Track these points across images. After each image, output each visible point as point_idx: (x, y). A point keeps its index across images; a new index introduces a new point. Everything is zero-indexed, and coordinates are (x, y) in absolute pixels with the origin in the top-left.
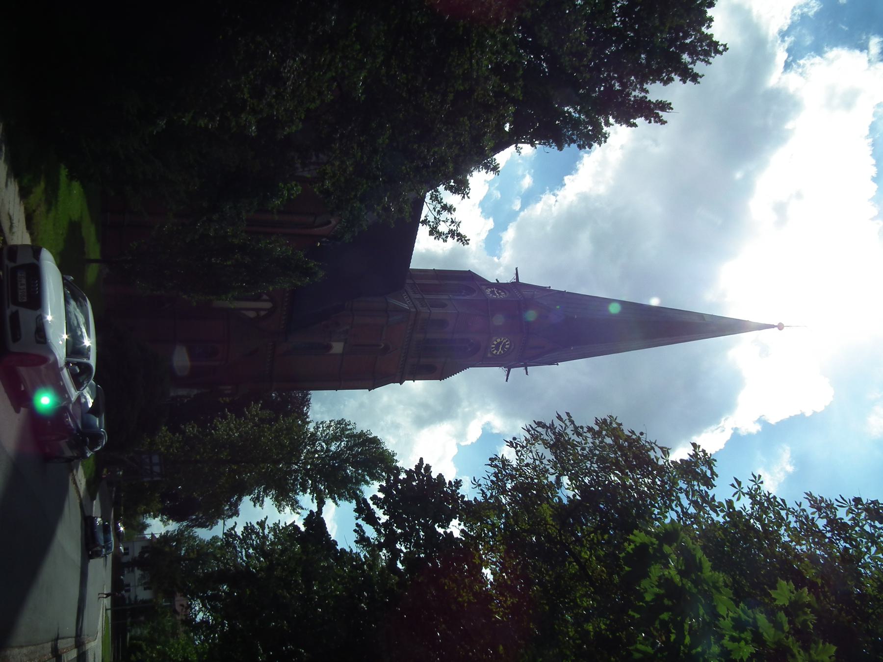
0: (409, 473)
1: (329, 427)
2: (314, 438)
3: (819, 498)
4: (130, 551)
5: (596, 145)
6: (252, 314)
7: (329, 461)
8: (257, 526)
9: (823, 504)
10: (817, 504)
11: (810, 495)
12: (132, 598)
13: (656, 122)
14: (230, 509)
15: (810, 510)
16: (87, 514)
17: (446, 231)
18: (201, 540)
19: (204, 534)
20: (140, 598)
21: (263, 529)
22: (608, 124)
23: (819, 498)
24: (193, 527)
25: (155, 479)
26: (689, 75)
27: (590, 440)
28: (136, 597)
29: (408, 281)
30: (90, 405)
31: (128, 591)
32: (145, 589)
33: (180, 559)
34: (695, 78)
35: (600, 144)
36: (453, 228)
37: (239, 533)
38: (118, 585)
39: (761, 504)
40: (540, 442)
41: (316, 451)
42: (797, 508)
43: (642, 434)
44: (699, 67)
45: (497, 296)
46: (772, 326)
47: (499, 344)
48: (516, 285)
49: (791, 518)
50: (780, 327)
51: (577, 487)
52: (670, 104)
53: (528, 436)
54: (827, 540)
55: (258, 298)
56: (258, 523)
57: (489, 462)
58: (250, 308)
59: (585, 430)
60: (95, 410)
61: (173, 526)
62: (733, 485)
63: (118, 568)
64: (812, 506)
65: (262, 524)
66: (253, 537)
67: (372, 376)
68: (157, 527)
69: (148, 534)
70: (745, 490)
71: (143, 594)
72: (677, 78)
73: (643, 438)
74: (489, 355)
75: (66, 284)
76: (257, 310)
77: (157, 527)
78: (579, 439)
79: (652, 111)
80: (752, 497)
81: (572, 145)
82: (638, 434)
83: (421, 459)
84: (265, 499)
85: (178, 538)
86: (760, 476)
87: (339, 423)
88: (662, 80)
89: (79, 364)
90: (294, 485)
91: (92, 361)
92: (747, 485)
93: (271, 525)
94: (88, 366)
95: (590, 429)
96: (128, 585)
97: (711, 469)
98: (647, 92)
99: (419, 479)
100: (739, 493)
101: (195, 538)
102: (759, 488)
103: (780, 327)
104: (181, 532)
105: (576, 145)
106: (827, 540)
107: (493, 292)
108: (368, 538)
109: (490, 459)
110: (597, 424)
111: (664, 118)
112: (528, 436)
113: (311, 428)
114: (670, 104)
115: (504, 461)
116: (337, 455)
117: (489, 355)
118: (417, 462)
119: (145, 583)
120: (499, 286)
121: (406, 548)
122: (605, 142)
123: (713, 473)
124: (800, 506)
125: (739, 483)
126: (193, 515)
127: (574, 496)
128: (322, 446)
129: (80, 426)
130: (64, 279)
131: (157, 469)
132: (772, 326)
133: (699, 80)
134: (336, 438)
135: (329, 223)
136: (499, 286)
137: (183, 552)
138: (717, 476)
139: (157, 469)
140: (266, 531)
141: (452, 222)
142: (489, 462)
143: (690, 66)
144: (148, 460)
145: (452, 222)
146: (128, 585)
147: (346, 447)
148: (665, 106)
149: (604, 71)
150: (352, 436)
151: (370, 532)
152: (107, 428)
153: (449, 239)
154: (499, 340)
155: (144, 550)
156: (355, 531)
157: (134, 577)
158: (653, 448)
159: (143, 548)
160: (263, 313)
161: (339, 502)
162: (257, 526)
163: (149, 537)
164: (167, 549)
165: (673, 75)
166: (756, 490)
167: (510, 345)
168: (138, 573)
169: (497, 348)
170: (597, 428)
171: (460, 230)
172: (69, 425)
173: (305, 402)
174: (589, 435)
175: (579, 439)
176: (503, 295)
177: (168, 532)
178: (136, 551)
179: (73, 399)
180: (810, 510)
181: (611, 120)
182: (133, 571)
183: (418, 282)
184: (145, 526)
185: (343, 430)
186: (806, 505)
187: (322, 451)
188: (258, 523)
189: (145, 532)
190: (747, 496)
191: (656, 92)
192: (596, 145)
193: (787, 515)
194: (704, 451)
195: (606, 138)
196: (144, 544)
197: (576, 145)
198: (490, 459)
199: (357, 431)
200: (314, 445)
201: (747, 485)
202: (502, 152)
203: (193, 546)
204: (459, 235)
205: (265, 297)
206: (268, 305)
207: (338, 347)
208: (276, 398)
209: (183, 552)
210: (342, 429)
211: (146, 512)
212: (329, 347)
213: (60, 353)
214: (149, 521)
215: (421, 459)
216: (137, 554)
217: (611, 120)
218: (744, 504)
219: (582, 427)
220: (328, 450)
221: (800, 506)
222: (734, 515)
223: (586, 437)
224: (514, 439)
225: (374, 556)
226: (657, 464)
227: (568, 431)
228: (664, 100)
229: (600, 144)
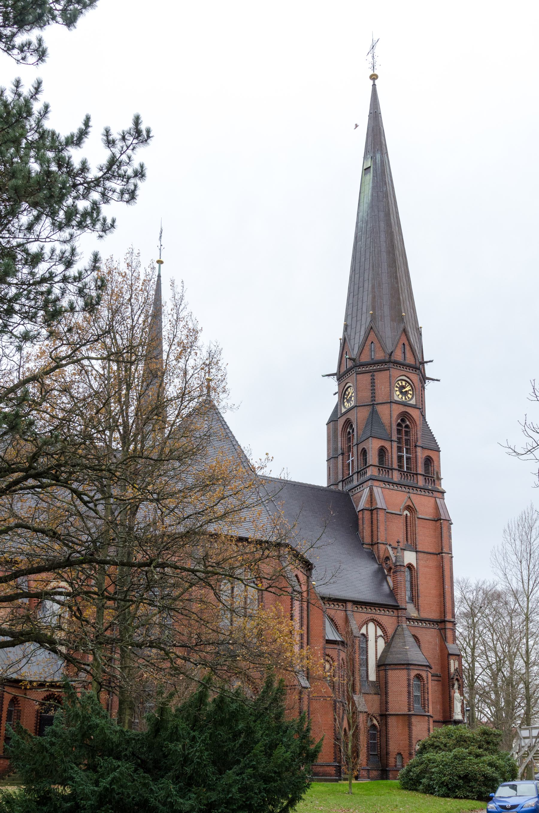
6: (381, 643)
46: (374, 85)
50: (374, 77)
55: (365, 637)
103: (374, 77)
107: (348, 401)
132: (374, 85)
154: (398, 393)
160: (380, 632)
205: (363, 631)
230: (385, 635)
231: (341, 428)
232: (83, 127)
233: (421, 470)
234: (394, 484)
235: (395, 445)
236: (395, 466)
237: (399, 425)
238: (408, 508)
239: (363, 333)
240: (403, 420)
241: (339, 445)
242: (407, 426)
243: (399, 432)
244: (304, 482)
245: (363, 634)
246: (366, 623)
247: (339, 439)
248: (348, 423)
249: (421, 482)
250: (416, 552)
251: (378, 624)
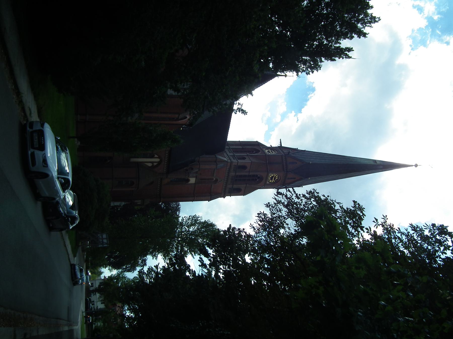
0: (224, 231)
1: (189, 219)
2: (181, 224)
3: (416, 226)
4: (94, 285)
5: (315, 71)
6: (150, 165)
7: (190, 236)
8: (154, 268)
9: (418, 229)
10: (414, 228)
11: (412, 225)
12: (96, 308)
13: (346, 58)
14: (142, 262)
15: (412, 232)
16: (72, 263)
17: (236, 109)
18: (128, 279)
19: (131, 275)
20: (99, 307)
21: (157, 269)
22: (321, 61)
23: (416, 226)
24: (124, 272)
25: (105, 246)
26: (362, 34)
27: (304, 201)
28: (97, 307)
29: (226, 147)
30: (71, 203)
31: (93, 304)
32: (102, 303)
33: (119, 288)
34: (365, 35)
35: (317, 71)
36: (240, 107)
37: (146, 271)
38: (88, 303)
39: (387, 229)
40: (281, 204)
41: (183, 232)
42: (406, 232)
43: (328, 196)
44: (367, 30)
45: (271, 153)
46: (412, 166)
47: (273, 176)
48: (281, 148)
49: (404, 237)
50: (416, 166)
51: (299, 226)
52: (352, 48)
53: (276, 202)
54: (419, 244)
55: (152, 157)
56: (155, 266)
57: (257, 215)
58: (149, 161)
59: (302, 196)
60: (73, 207)
61: (115, 272)
62: (374, 221)
63: (89, 292)
64: (412, 230)
65: (157, 267)
66: (153, 273)
67: (209, 195)
68: (107, 272)
69: (102, 277)
70: (380, 223)
71: (101, 306)
72: (356, 36)
73: (329, 198)
74: (268, 183)
75: (57, 142)
76: (152, 162)
77: (107, 272)
78: (299, 201)
79: (343, 53)
80: (383, 226)
81: (303, 73)
82: (326, 196)
83: (230, 225)
84: (158, 256)
85: (118, 277)
86: (386, 216)
87: (194, 217)
88: (348, 38)
89: (63, 178)
90: (172, 248)
91: (70, 178)
92: (380, 221)
93: (161, 267)
94: (68, 180)
95: (304, 196)
96: (94, 302)
97: (362, 212)
98: (340, 43)
99: (229, 234)
100: (377, 226)
101: (125, 278)
102: (386, 221)
103: (416, 166)
104: (118, 275)
105: (305, 73)
106: (419, 244)
107: (269, 151)
108: (205, 264)
109: (258, 214)
110: (307, 193)
111: (350, 55)
112: (276, 202)
113: (180, 219)
114: (352, 48)
115: (265, 215)
116: (193, 233)
117: (268, 183)
118: (228, 226)
119: (101, 301)
120: (272, 148)
121: (224, 268)
122: (320, 69)
123: (363, 214)
124: (407, 230)
125: (377, 220)
126: (124, 265)
127: (298, 230)
128: (186, 229)
129: (66, 212)
130: (56, 138)
131: (105, 241)
132: (412, 166)
133: (367, 36)
134: (192, 225)
135: (186, 117)
136: (272, 148)
137: (120, 285)
138: (365, 216)
139: (105, 241)
140: (159, 270)
141: (239, 104)
142: (257, 215)
143: (362, 30)
144: (101, 237)
145: (239, 104)
146: (94, 302)
147: (198, 229)
148: (350, 50)
149: (319, 35)
150: (200, 223)
151: (207, 261)
152: (79, 214)
153: (238, 112)
154: (272, 175)
155: (101, 284)
156: (199, 260)
157: (96, 297)
158: (333, 203)
159: (100, 283)
160: (155, 164)
161: (194, 256)
162: (154, 268)
163: (103, 278)
164: (112, 283)
165: (353, 35)
166: (385, 223)
167: (278, 177)
168: (98, 295)
169: (272, 179)
170: (307, 195)
171: (243, 108)
172: (61, 211)
173: (178, 209)
174: (303, 198)
175: (299, 201)
176: (274, 153)
177: (112, 275)
178: (97, 285)
179: (62, 197)
180: (412, 232)
181: (323, 59)
182: (95, 294)
183: (231, 147)
184: (101, 273)
185: (196, 221)
186: (410, 230)
187: (185, 231)
188: (155, 266)
189: (101, 276)
190: (381, 226)
191: (345, 43)
192: (315, 71)
193: (401, 235)
194: (358, 204)
195: (320, 67)
196: (101, 281)
197: (305, 73)
198: (258, 214)
199: (203, 221)
200: (182, 228)
201: (380, 221)
202: (271, 81)
203: (124, 281)
204: (242, 110)
205: (156, 156)
206: (158, 160)
207: (192, 180)
208: (164, 207)
209: (120, 285)
210: (195, 220)
211: (100, 266)
212: (188, 180)
213: (55, 174)
214: (103, 270)
215: (230, 225)
216: (97, 286)
217: (323, 59)
218: (380, 231)
219: (300, 195)
220: (189, 231)
221: (407, 230)
222: (375, 235)
223: (302, 199)
224: (269, 203)
225: (209, 273)
226: (334, 209)
227: (294, 197)
228: (349, 47)
229: (317, 71)
230: (153, 167)
231: (253, 148)
232: (269, 114)
233: (235, 186)
234: (229, 173)
235: (247, 174)
236: (237, 174)
237: (257, 176)
238: (217, 180)
239: (301, 159)
240: (259, 178)
241: (247, 147)
242: (256, 180)
243: (254, 176)
244: (241, 140)
245: (154, 156)
246: (159, 157)
247: (252, 147)
248: (258, 151)
249: (229, 186)
250: (195, 184)
251: (159, 163)
